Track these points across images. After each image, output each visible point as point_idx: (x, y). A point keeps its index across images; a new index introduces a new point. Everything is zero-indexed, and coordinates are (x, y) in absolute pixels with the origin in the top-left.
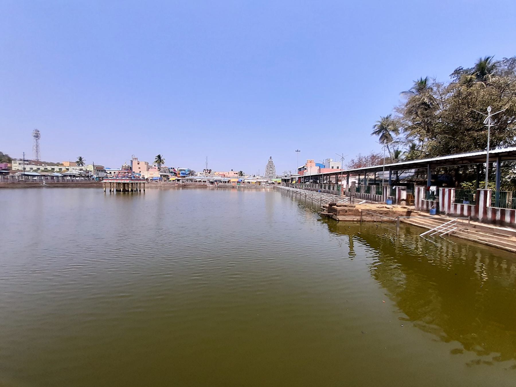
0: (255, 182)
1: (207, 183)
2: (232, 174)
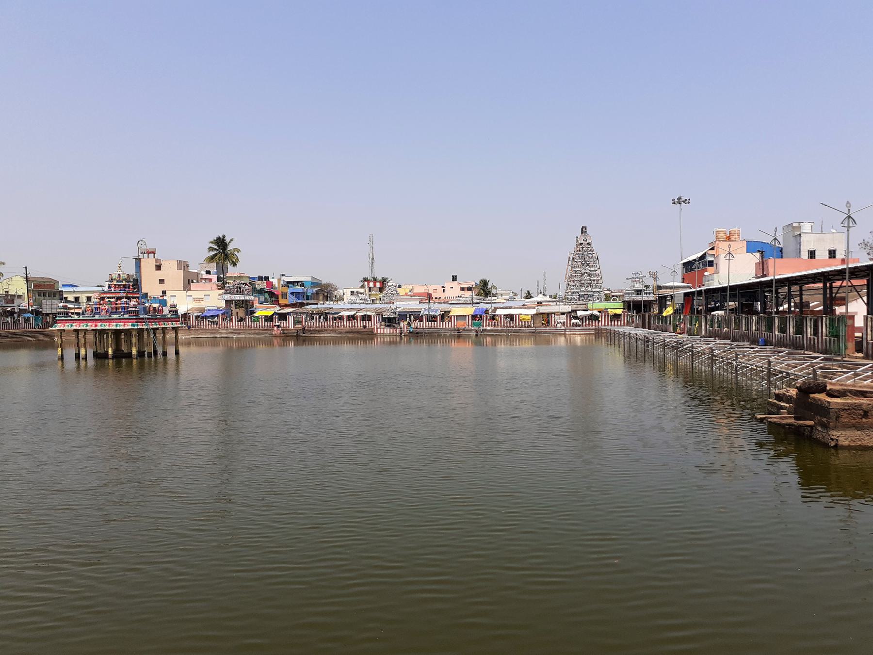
0: (534, 317)
2: (453, 291)
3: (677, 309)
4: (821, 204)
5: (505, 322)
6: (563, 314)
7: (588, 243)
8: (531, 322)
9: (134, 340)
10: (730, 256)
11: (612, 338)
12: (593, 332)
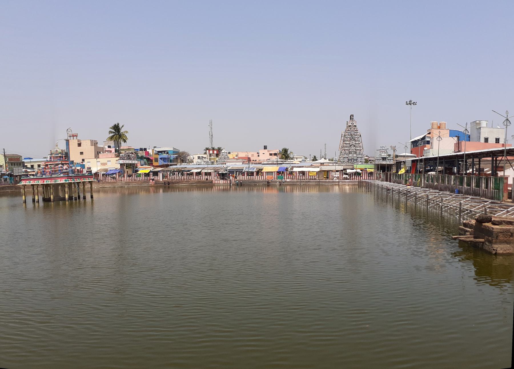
0: (318, 173)
1: (214, 178)
2: (265, 156)
3: (407, 170)
4: (493, 111)
5: (299, 176)
6: (337, 171)
7: (354, 126)
8: (316, 176)
9: (67, 190)
10: (440, 138)
11: (368, 186)
12: (357, 183)
